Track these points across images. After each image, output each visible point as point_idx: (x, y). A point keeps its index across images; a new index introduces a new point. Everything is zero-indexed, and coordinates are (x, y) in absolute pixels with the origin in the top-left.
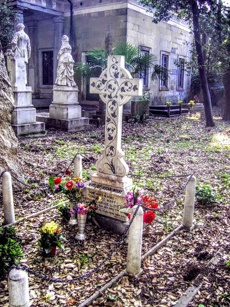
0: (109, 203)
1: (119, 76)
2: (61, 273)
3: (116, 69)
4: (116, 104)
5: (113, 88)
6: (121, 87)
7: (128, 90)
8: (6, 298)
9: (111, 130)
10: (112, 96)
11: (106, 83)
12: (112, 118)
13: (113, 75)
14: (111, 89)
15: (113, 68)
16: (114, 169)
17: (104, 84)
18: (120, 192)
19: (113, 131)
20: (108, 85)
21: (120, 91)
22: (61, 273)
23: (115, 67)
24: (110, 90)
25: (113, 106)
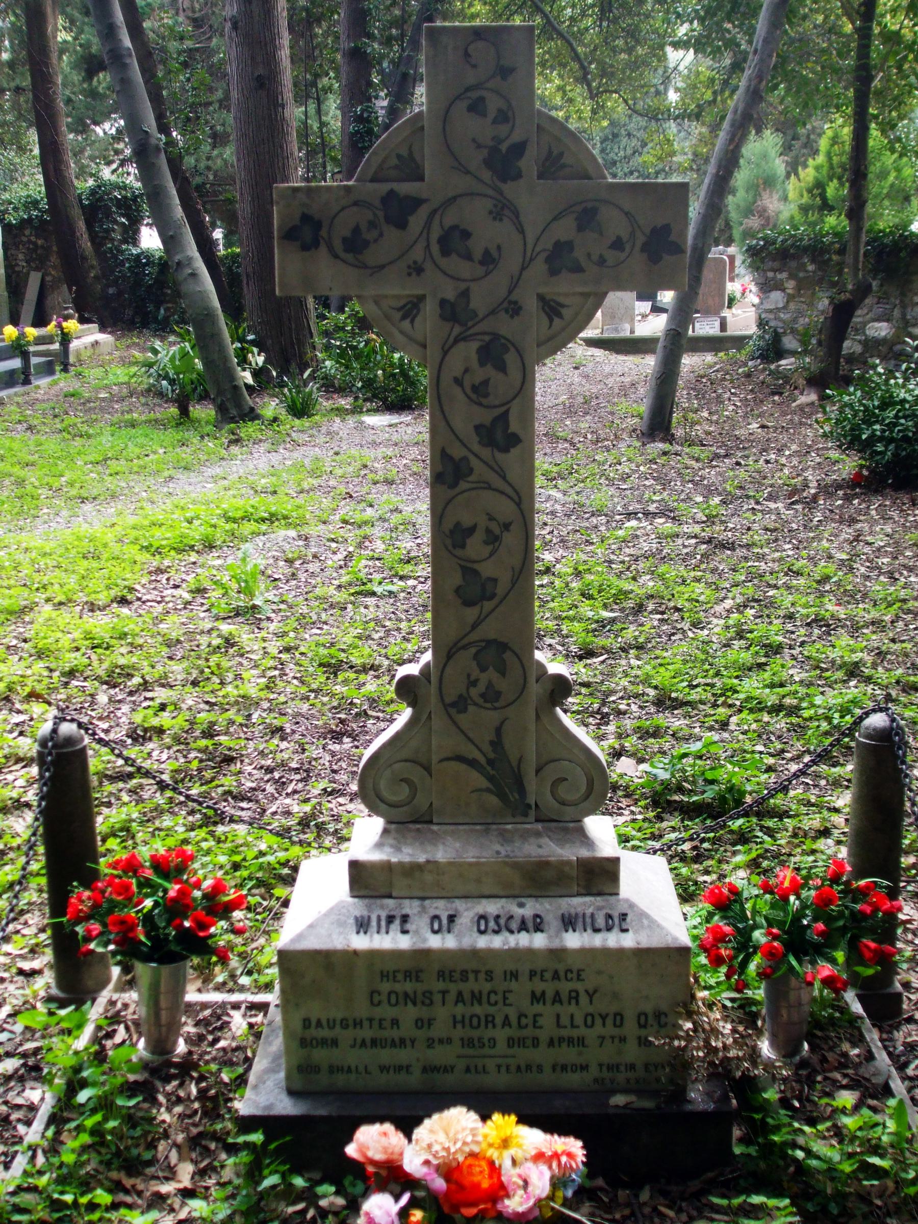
0: (547, 1011)
1: (529, 163)
2: (804, 872)
3: (504, 117)
4: (511, 358)
5: (478, 254)
6: (547, 243)
7: (602, 261)
8: (695, 932)
9: (479, 536)
10: (479, 302)
11: (416, 221)
12: (486, 453)
13: (475, 159)
14: (468, 257)
15: (477, 107)
16: (449, 200)
17: (402, 225)
18: (589, 178)
19: (493, 539)
20: (436, 233)
21: (539, 267)
22: (804, 872)
23: (493, 104)
24: (454, 264)
25: (489, 371)
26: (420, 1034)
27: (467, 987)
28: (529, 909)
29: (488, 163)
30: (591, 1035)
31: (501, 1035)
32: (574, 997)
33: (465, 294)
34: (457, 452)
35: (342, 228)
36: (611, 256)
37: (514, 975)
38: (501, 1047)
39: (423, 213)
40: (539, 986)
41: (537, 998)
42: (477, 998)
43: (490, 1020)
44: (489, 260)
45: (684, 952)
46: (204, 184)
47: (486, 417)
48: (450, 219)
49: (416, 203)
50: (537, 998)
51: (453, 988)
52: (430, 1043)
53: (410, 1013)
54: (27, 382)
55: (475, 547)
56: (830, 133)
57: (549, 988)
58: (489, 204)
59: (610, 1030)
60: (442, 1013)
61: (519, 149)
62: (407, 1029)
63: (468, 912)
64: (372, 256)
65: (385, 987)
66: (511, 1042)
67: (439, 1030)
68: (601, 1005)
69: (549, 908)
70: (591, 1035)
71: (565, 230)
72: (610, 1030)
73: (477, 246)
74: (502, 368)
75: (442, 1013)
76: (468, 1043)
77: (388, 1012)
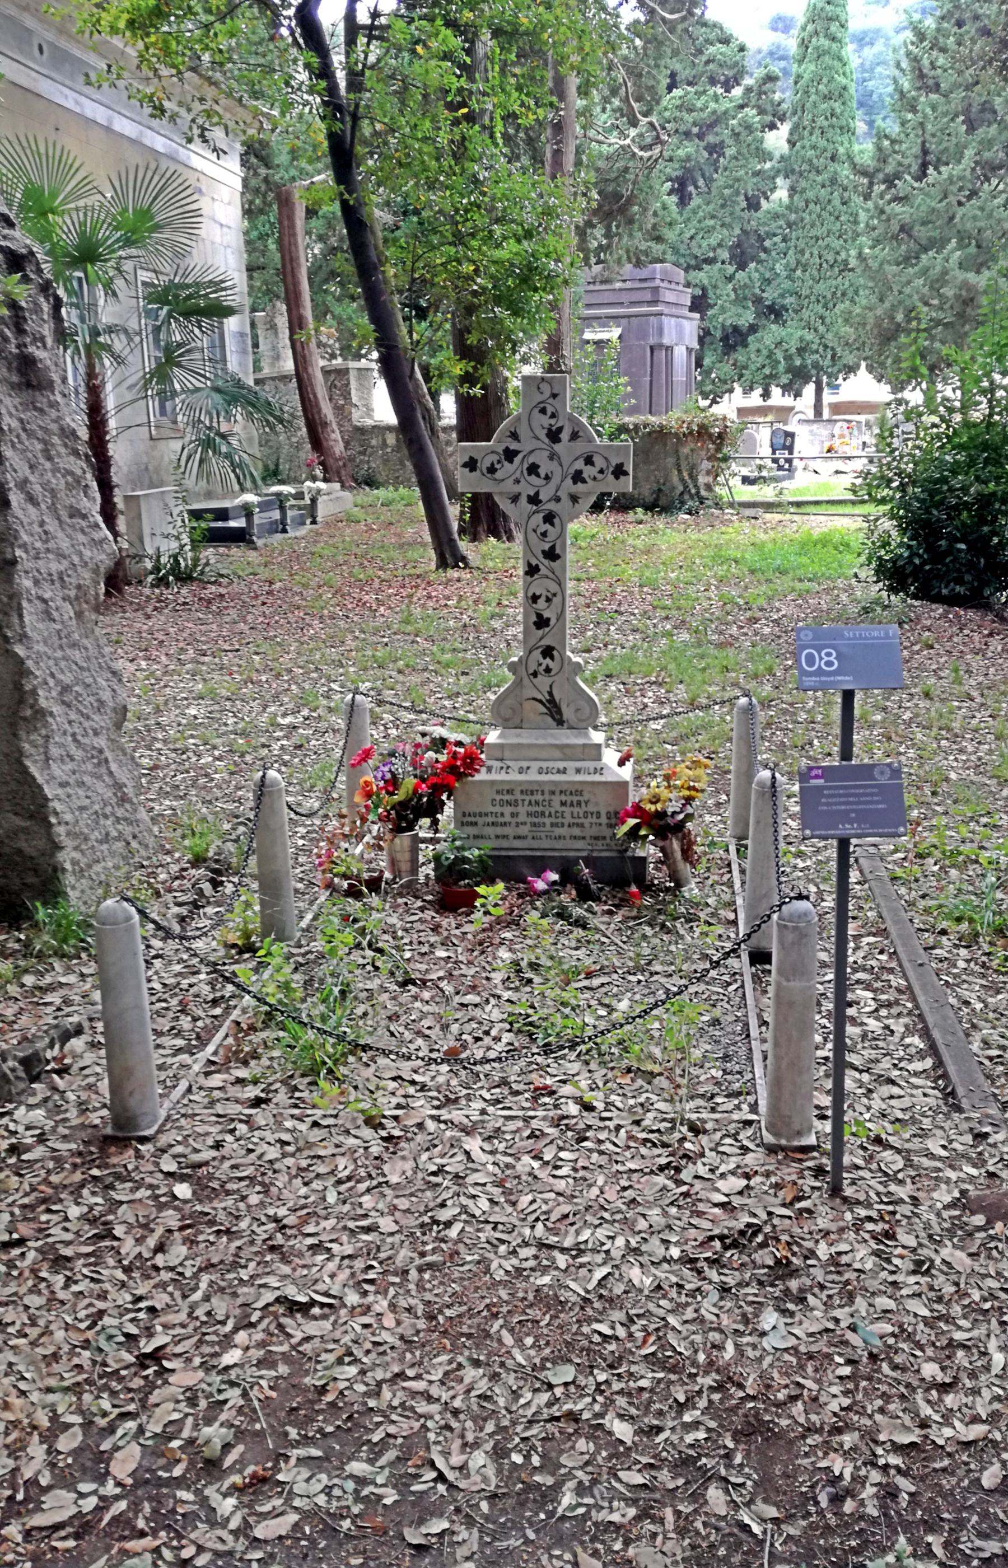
0: (567, 810)
1: (565, 436)
4: (556, 521)
6: (572, 471)
11: (517, 460)
13: (542, 434)
15: (543, 411)
17: (511, 461)
19: (548, 600)
20: (526, 466)
21: (569, 481)
24: (533, 479)
25: (548, 526)
26: (514, 821)
27: (533, 798)
28: (561, 765)
29: (548, 435)
30: (586, 822)
31: (547, 821)
32: (579, 803)
33: (537, 493)
34: (534, 562)
35: (487, 463)
36: (600, 476)
37: (553, 793)
38: (548, 827)
39: (520, 456)
40: (564, 798)
41: (563, 804)
42: (537, 803)
43: (543, 814)
44: (547, 478)
45: (626, 783)
46: (915, 597)
47: (546, 547)
48: (531, 460)
49: (516, 453)
50: (563, 804)
51: (527, 798)
52: (517, 825)
53: (508, 810)
54: (284, 531)
55: (541, 603)
56: (431, 754)
57: (569, 799)
58: (547, 453)
59: (595, 820)
60: (522, 810)
61: (560, 429)
62: (507, 818)
63: (535, 765)
64: (498, 475)
65: (498, 797)
66: (552, 825)
67: (522, 818)
68: (591, 808)
69: (571, 765)
70: (586, 822)
71: (580, 465)
72: (595, 820)
73: (542, 472)
74: (552, 524)
75: (522, 810)
76: (534, 825)
77: (498, 809)
